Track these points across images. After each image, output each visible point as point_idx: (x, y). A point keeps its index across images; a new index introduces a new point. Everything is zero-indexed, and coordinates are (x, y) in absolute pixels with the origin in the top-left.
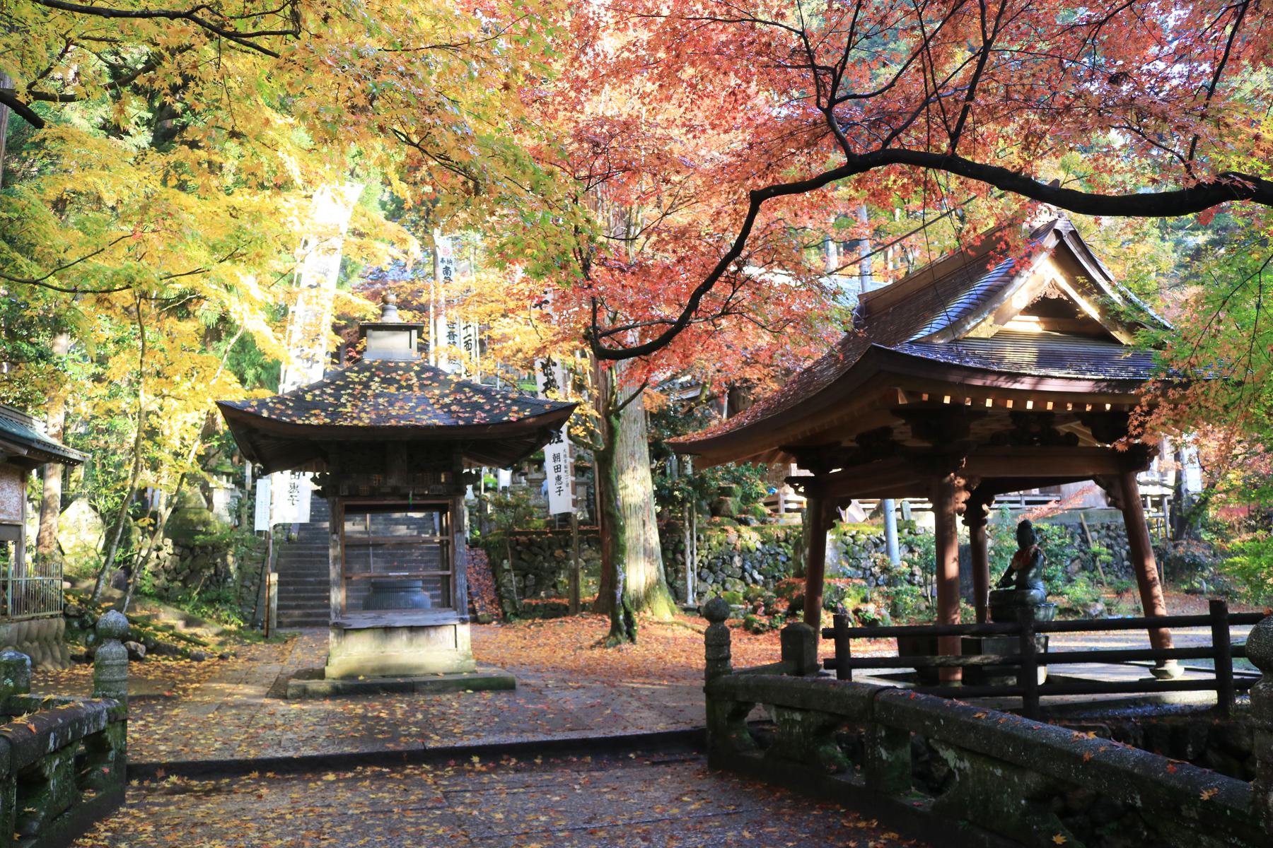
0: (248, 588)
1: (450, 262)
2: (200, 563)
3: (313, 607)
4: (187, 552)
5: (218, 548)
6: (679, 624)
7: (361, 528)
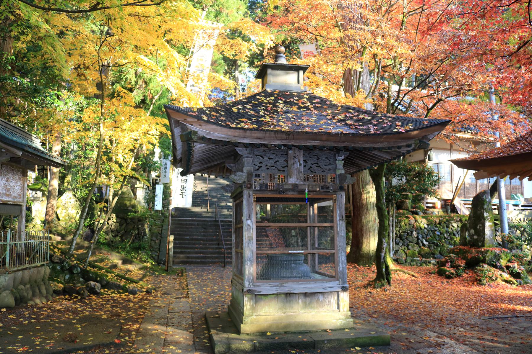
0: (155, 241)
1: (245, 86)
2: (132, 229)
3: (189, 253)
4: (123, 221)
5: (141, 220)
6: (400, 271)
7: (205, 210)
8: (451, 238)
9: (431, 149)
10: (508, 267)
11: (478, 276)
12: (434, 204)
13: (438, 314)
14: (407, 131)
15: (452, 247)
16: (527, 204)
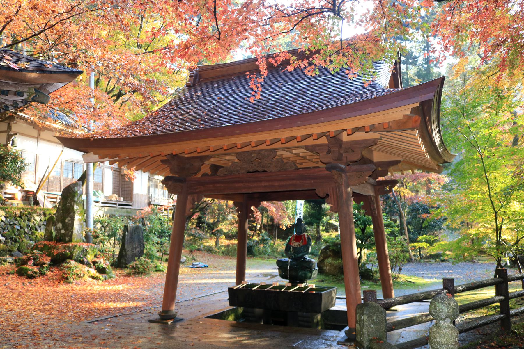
8: (32, 233)
9: (16, 134)
10: (94, 263)
11: (65, 273)
12: (14, 195)
13: (27, 327)
14: (21, 70)
15: (33, 243)
16: (106, 201)
